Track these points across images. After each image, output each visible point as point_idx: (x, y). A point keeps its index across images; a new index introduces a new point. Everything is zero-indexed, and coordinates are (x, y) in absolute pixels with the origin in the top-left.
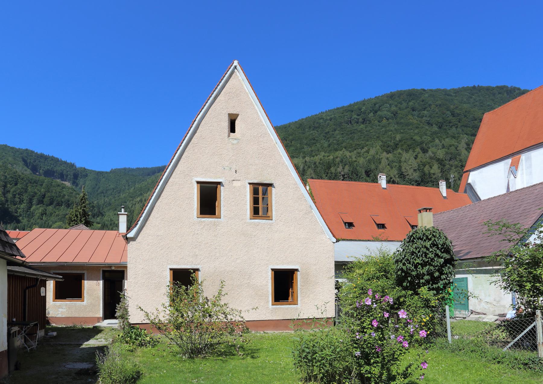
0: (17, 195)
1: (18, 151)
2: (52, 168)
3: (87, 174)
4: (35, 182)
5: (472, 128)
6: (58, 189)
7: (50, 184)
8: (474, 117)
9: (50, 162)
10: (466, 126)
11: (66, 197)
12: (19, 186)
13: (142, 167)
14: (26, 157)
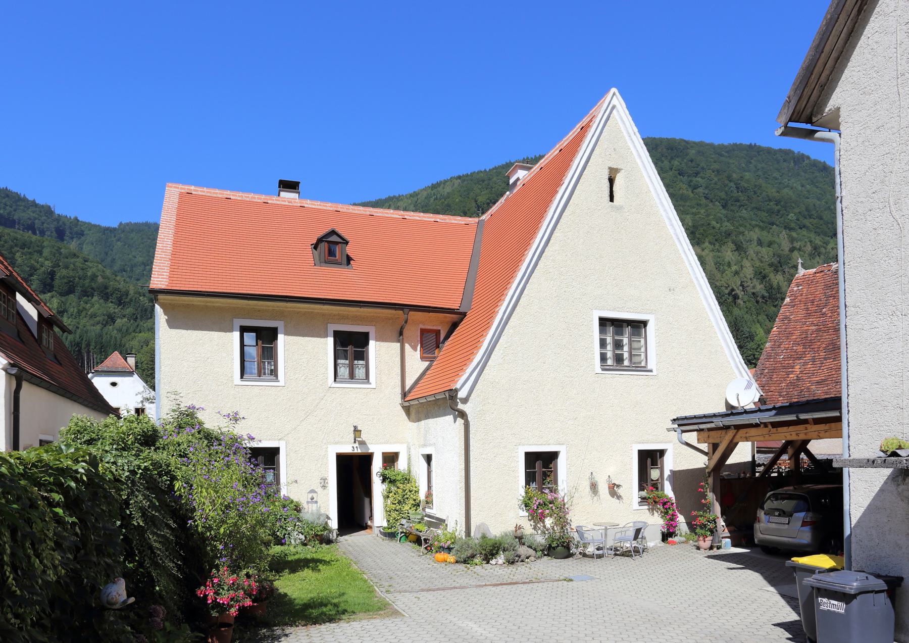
2: (9, 214)
3: (83, 231)
5: (767, 213)
7: (57, 250)
8: (768, 196)
10: (759, 209)
11: (100, 279)
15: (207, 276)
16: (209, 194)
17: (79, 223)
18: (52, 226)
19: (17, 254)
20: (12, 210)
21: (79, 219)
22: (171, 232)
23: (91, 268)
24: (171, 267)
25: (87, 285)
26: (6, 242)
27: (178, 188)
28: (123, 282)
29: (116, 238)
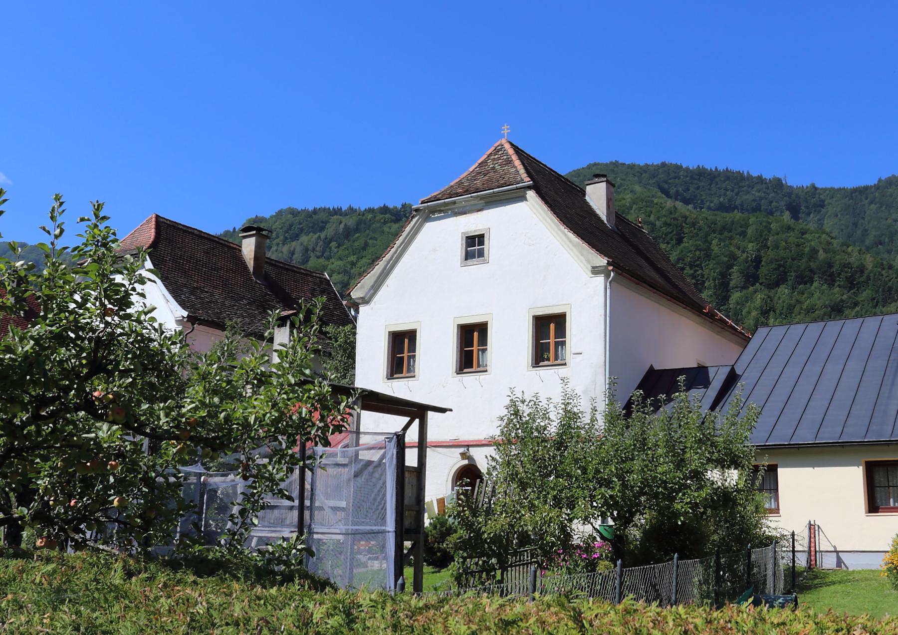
0: (688, 268)
1: (645, 172)
2: (730, 200)
3: (823, 201)
4: (725, 228)
6: (792, 237)
7: (766, 227)
9: (724, 185)
11: (821, 255)
12: (687, 243)
14: (666, 182)
18: (783, 203)
19: (713, 242)
20: (734, 194)
21: (816, 186)
23: (809, 241)
25: (803, 267)
26: (700, 230)
29: (869, 199)
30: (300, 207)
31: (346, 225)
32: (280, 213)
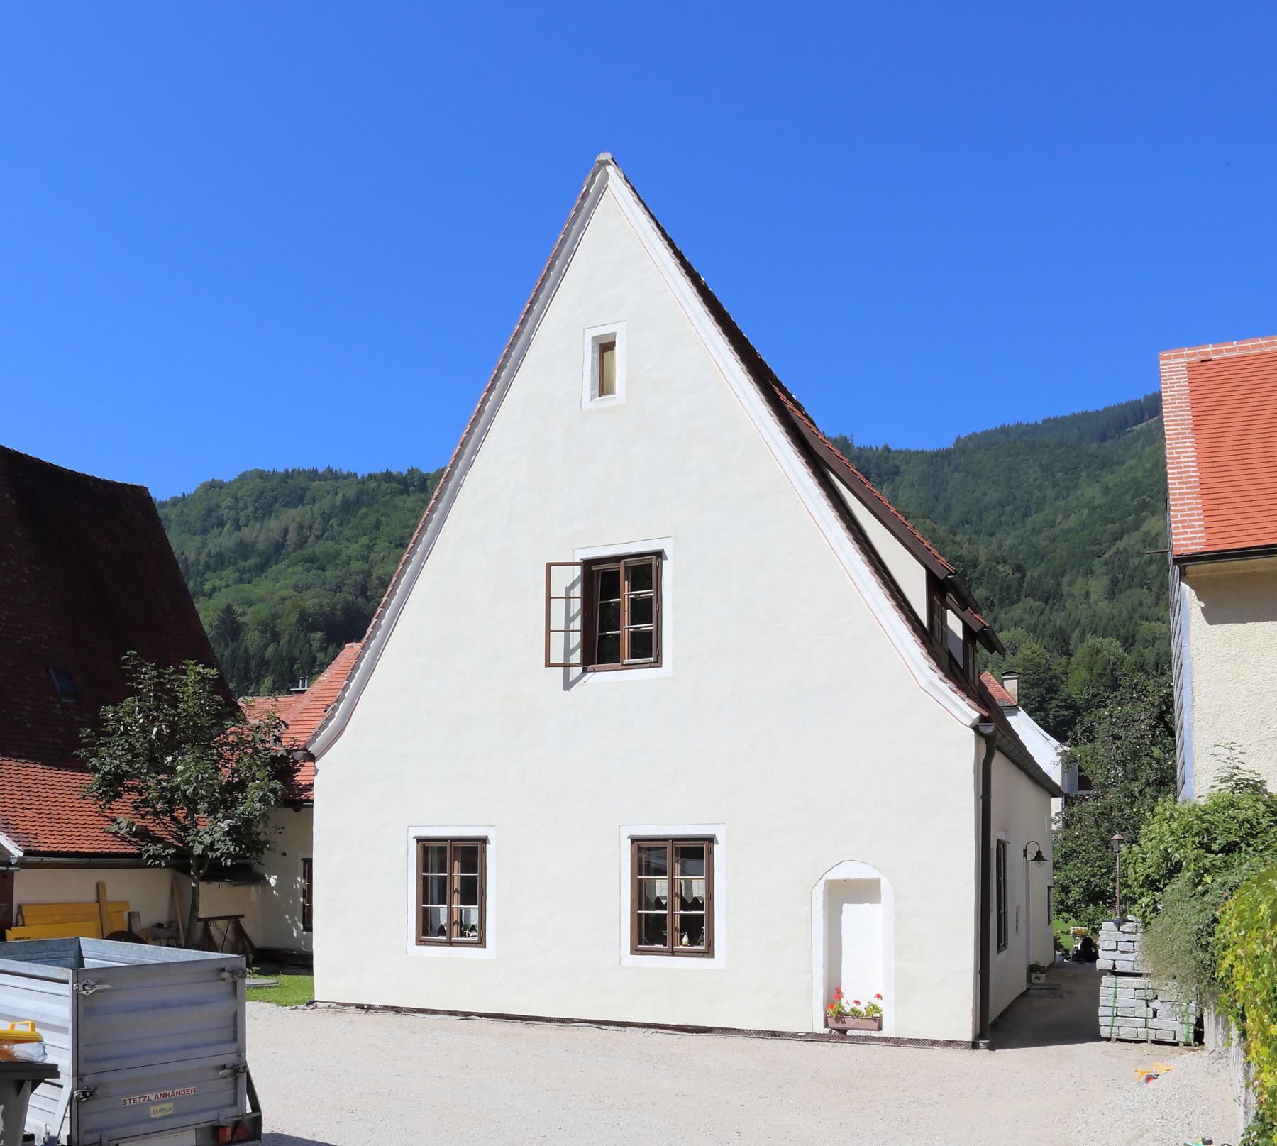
3: (898, 468)
13: (1067, 413)
15: (1228, 506)
16: (1245, 352)
17: (891, 455)
22: (1189, 442)
24: (1205, 508)
27: (1182, 356)
28: (967, 544)
29: (952, 466)
30: (268, 467)
31: (344, 496)
32: (243, 477)
